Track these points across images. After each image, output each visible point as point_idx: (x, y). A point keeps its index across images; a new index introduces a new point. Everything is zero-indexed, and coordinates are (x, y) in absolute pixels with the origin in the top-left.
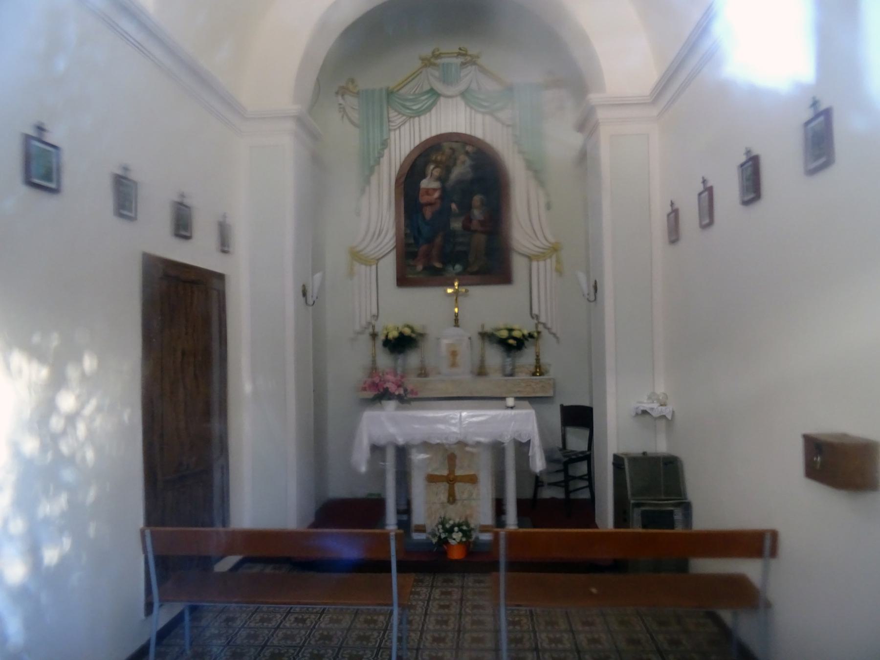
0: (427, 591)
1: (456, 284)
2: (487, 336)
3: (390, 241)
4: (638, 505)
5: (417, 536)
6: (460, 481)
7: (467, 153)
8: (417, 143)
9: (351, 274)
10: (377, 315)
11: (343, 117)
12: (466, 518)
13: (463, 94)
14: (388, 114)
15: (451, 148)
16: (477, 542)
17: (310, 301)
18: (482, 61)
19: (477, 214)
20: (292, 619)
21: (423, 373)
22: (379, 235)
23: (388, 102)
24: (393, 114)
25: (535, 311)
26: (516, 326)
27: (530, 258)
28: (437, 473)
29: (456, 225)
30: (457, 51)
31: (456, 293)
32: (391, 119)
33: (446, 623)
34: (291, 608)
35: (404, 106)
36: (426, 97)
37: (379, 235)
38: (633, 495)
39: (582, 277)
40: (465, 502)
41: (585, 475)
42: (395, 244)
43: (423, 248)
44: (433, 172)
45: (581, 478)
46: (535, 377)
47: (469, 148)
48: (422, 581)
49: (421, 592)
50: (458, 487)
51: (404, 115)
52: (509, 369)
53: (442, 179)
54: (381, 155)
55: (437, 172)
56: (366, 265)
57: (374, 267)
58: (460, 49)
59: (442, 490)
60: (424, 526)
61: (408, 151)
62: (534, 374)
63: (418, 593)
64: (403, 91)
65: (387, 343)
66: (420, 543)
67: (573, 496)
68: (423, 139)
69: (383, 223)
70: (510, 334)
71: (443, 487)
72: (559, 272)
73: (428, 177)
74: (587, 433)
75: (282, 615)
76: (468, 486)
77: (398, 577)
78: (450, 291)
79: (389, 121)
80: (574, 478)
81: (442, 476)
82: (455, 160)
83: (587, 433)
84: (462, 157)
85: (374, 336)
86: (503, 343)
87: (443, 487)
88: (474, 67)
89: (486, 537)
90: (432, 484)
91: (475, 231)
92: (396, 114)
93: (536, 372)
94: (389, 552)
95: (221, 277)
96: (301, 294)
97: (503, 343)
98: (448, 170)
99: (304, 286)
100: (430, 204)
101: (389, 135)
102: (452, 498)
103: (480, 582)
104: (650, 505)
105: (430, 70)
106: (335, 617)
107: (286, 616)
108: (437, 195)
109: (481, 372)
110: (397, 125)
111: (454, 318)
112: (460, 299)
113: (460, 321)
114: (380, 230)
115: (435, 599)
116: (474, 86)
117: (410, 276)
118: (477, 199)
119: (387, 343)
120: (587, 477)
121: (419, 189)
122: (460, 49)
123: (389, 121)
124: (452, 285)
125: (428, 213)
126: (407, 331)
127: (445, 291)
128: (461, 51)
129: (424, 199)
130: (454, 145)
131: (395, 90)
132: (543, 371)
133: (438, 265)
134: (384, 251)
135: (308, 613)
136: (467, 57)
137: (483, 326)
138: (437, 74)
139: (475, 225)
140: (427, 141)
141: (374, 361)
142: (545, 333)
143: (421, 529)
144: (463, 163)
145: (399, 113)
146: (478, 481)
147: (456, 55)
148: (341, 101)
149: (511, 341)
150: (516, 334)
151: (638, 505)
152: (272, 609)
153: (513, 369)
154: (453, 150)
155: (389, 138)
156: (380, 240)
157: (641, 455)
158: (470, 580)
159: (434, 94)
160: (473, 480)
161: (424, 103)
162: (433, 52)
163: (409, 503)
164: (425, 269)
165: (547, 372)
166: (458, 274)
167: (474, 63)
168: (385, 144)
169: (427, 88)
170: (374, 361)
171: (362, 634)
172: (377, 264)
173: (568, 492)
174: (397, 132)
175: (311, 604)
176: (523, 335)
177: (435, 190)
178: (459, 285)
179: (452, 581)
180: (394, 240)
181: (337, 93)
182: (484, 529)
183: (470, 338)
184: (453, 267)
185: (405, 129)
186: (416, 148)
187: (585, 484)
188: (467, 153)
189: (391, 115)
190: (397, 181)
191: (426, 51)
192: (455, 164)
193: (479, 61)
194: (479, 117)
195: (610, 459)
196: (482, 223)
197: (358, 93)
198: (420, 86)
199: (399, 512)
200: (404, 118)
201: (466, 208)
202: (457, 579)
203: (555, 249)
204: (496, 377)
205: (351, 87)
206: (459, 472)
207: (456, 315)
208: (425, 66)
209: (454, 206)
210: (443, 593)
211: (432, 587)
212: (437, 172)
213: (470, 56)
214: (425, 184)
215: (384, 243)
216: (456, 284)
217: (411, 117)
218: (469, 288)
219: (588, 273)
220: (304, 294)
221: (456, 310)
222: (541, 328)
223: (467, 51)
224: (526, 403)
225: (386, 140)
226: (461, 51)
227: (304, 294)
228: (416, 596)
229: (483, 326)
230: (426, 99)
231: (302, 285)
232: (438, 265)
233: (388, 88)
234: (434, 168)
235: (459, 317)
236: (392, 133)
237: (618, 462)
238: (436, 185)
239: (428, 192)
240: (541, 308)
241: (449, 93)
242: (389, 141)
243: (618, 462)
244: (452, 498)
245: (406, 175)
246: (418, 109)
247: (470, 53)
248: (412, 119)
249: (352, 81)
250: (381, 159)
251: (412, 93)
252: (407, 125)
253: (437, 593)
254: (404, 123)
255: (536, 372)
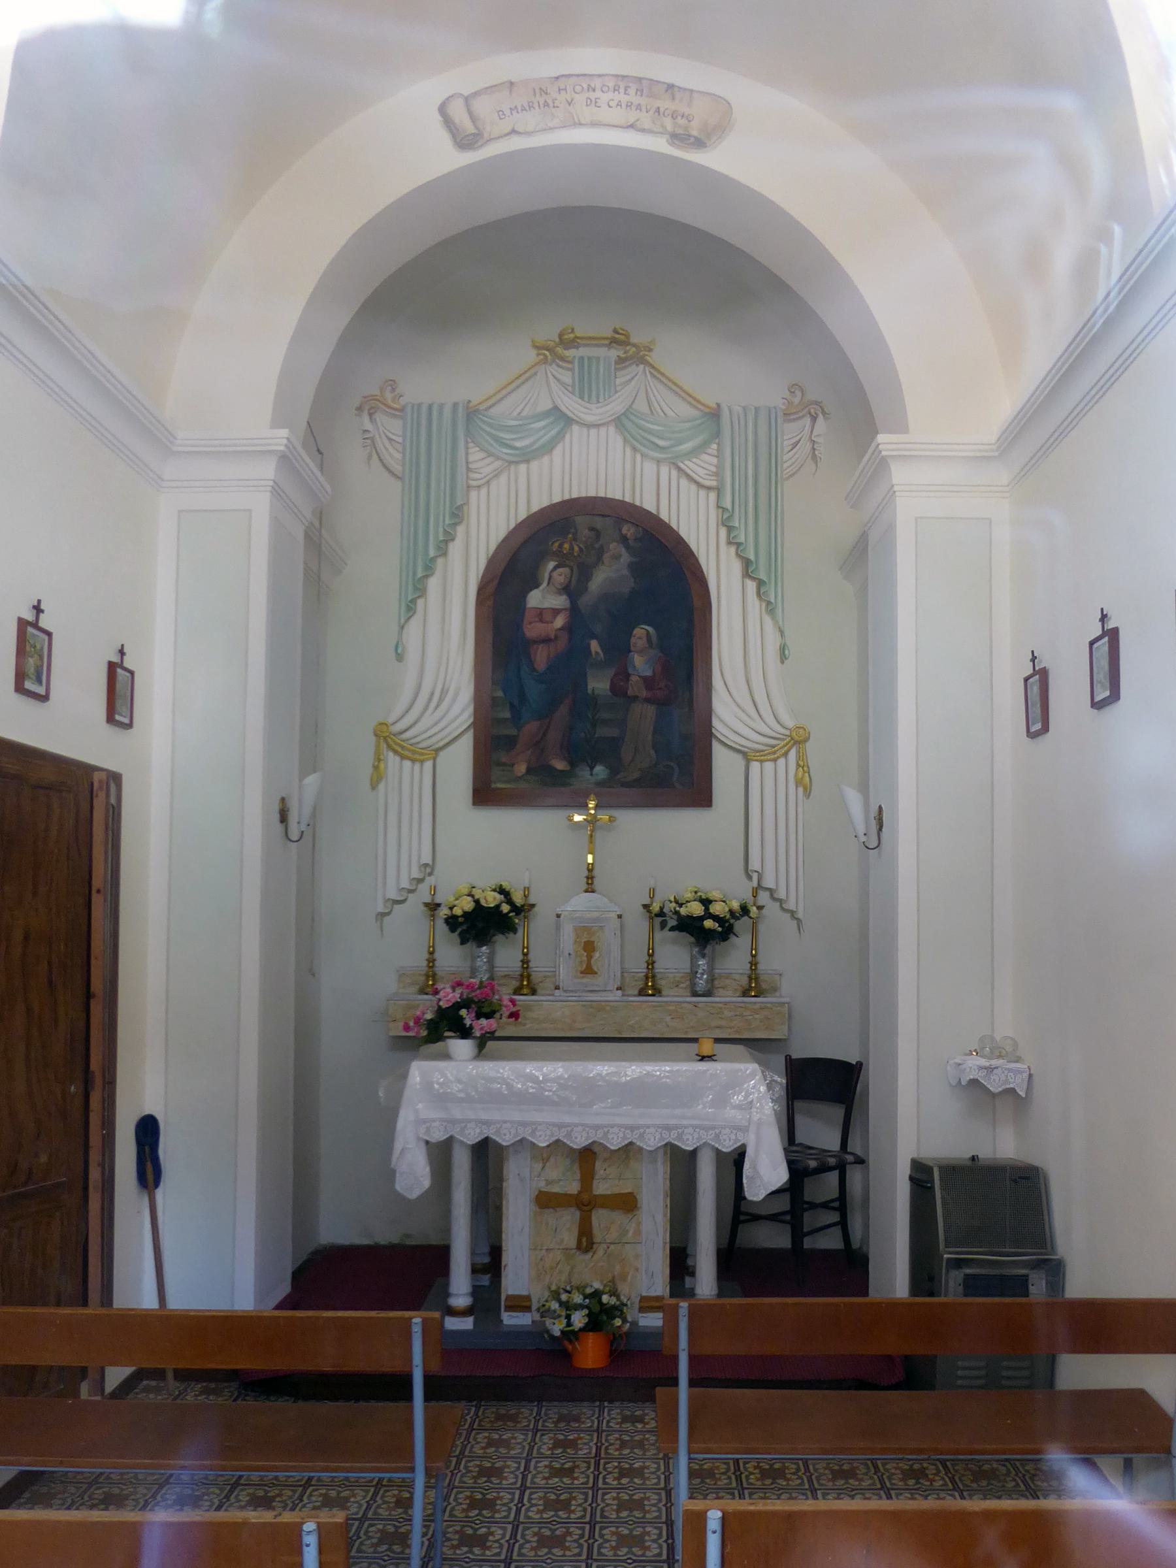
0: (525, 1440)
1: (592, 804)
2: (658, 917)
3: (463, 711)
4: (958, 1264)
5: (510, 1319)
6: (603, 1206)
7: (624, 540)
8: (522, 515)
9: (377, 777)
10: (430, 862)
11: (370, 457)
12: (613, 1281)
13: (619, 422)
14: (467, 454)
15: (592, 529)
16: (635, 1333)
17: (294, 834)
18: (653, 358)
19: (641, 664)
20: (244, 1498)
21: (526, 983)
22: (441, 700)
23: (468, 433)
24: (476, 455)
25: (755, 864)
26: (715, 894)
27: (747, 756)
28: (556, 1189)
29: (599, 684)
30: (610, 334)
31: (592, 821)
32: (471, 466)
33: (566, 1505)
34: (171, 1475)
35: (497, 439)
36: (542, 424)
37: (441, 700)
38: (948, 1244)
39: (854, 799)
40: (612, 1247)
41: (832, 1201)
42: (471, 720)
43: (531, 727)
44: (555, 574)
45: (825, 1205)
46: (746, 999)
47: (628, 530)
48: (514, 1418)
49: (513, 1441)
50: (600, 1218)
51: (498, 458)
52: (702, 983)
53: (572, 591)
54: (450, 538)
55: (561, 575)
56: (413, 761)
57: (428, 765)
58: (615, 331)
59: (567, 1222)
60: (528, 1298)
61: (502, 534)
62: (745, 993)
63: (506, 1444)
64: (494, 411)
65: (452, 922)
66: (517, 1333)
67: (808, 1243)
68: (535, 508)
69: (448, 678)
70: (707, 909)
71: (568, 1219)
72: (805, 785)
73: (545, 584)
74: (838, 1112)
75: (222, 1490)
76: (618, 1217)
77: (426, 1409)
78: (578, 818)
79: (468, 469)
80: (813, 1206)
81: (566, 1195)
82: (601, 551)
83: (838, 1112)
84: (614, 547)
85: (433, 907)
86: (689, 926)
87: (568, 1219)
88: (642, 366)
89: (653, 1320)
90: (547, 1211)
91: (635, 698)
92: (482, 455)
93: (750, 988)
94: (410, 1360)
95: (116, 778)
96: (277, 817)
97: (689, 926)
98: (585, 572)
99: (283, 799)
100: (547, 640)
101: (468, 495)
102: (586, 1241)
103: (634, 1420)
104: (980, 1262)
105: (553, 369)
106: (333, 1494)
107: (231, 1491)
108: (559, 622)
109: (650, 986)
110: (485, 477)
111: (586, 873)
112: (598, 835)
113: (596, 881)
114: (443, 689)
115: (542, 1456)
116: (641, 406)
117: (499, 785)
118: (641, 633)
119: (452, 922)
120: (836, 1204)
121: (524, 609)
122: (615, 331)
123: (468, 469)
124: (583, 807)
125: (541, 657)
126: (491, 899)
127: (570, 819)
128: (617, 336)
129: (533, 630)
130: (598, 522)
131: (482, 407)
132: (764, 986)
133: (560, 765)
134: (450, 734)
135: (279, 1485)
136: (628, 348)
137: (652, 893)
138: (566, 377)
139: (635, 687)
140: (542, 511)
141: (431, 961)
142: (772, 909)
143: (520, 1304)
144: (617, 557)
145: (490, 455)
146: (639, 1205)
147: (607, 342)
148: (368, 425)
149: (709, 924)
150: (717, 909)
151: (958, 1264)
152: (132, 1475)
153: (711, 980)
154: (597, 533)
155: (467, 503)
156: (439, 713)
157: (969, 1163)
158: (613, 1414)
159: (562, 419)
160: (627, 1203)
161: (541, 433)
162: (561, 336)
163: (496, 1252)
164: (529, 771)
165: (775, 989)
166: (600, 784)
167: (643, 361)
168: (458, 515)
169: (545, 405)
170: (431, 961)
171: (391, 1529)
172: (435, 760)
173: (798, 1235)
174: (484, 491)
175: (145, 1467)
176: (731, 912)
177: (556, 612)
178: (596, 807)
179: (577, 1419)
180: (471, 709)
181: (360, 409)
182: (649, 1304)
183: (620, 917)
184: (592, 768)
185: (500, 486)
186: (519, 526)
187: (835, 1217)
188: (624, 540)
189: (471, 459)
190: (481, 590)
191: (548, 332)
192: (600, 559)
193: (653, 358)
194: (649, 468)
195: (903, 1171)
196: (648, 682)
197: (402, 410)
198: (532, 401)
199: (475, 1270)
200: (498, 463)
201: (618, 650)
202: (588, 1413)
203: (797, 740)
204: (675, 996)
205: (389, 396)
206: (601, 1188)
207: (590, 869)
208: (545, 361)
209: (595, 646)
210: (557, 1444)
211: (536, 1431)
212: (561, 575)
213: (634, 345)
214: (536, 599)
215: (451, 716)
216: (592, 804)
217: (511, 463)
218: (616, 813)
219: (864, 788)
220: (284, 817)
221: (590, 859)
222: (763, 898)
223: (627, 336)
224: (740, 1048)
225: (460, 508)
226: (617, 336)
227: (284, 817)
228: (503, 1450)
229: (652, 893)
230: (544, 428)
231: (279, 798)
232: (560, 765)
233: (469, 402)
234: (556, 568)
235: (596, 873)
236: (473, 494)
237: (921, 1175)
238: (560, 601)
239: (541, 615)
240: (762, 858)
241: (590, 419)
242: (465, 508)
243: (921, 1175)
244: (586, 1241)
245: (498, 578)
246: (527, 447)
247: (633, 340)
248: (513, 467)
249: (392, 384)
250: (451, 545)
251: (515, 414)
252: (503, 478)
253: (545, 1444)
254: (497, 475)
255: (750, 988)
